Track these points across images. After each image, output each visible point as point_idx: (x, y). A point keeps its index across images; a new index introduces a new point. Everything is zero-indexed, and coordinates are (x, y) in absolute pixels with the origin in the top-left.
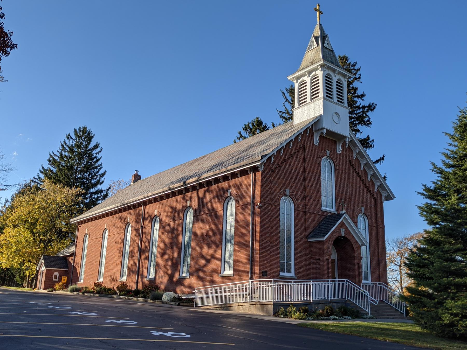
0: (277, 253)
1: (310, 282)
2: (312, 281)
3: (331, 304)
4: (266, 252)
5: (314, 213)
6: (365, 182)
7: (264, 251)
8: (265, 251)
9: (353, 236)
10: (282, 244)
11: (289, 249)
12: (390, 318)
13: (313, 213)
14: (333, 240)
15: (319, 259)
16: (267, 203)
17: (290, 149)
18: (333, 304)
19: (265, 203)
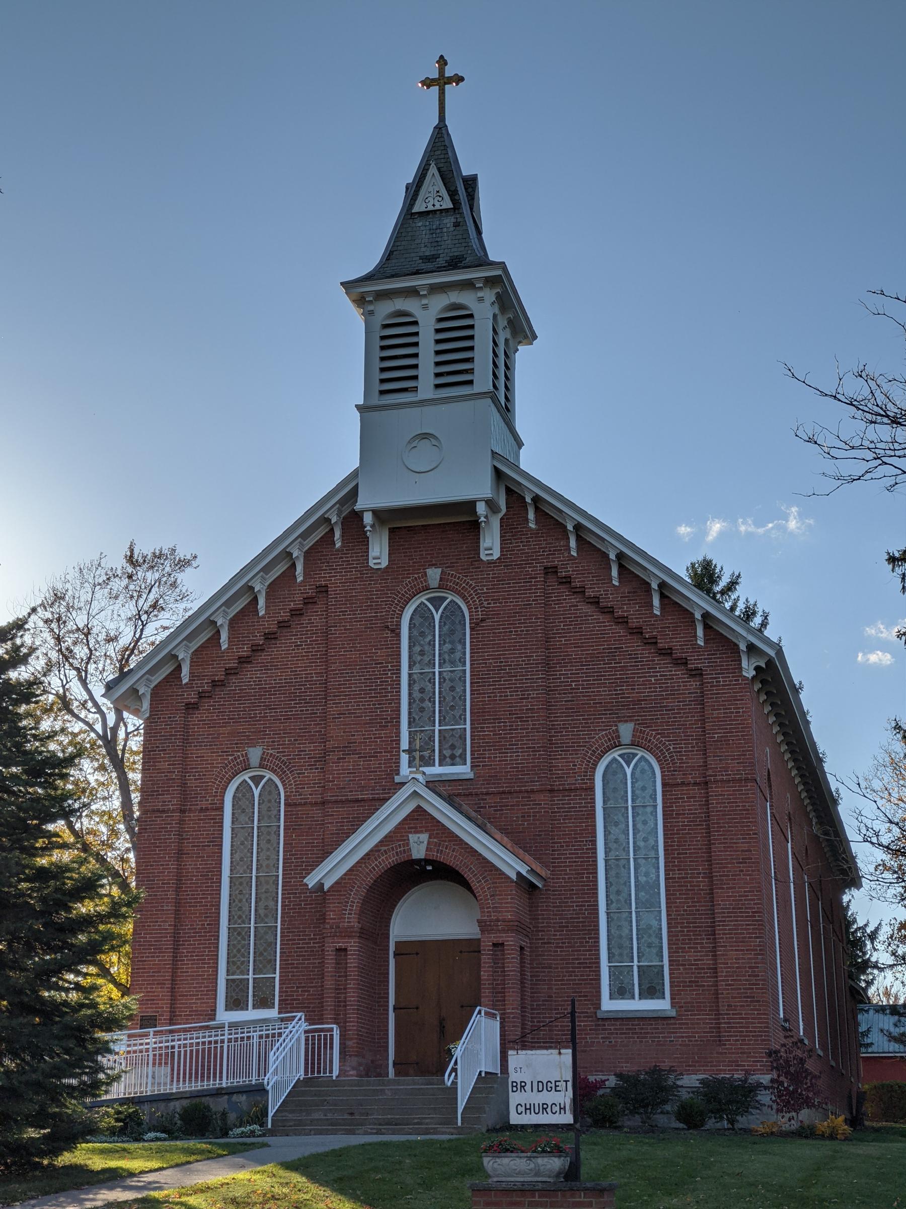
0: (207, 955)
1: (146, 1035)
2: (155, 1032)
3: (226, 1097)
4: (157, 957)
5: (363, 800)
6: (634, 625)
7: (146, 957)
8: (154, 957)
9: (367, 854)
10: (239, 921)
11: (266, 933)
12: (357, 1132)
13: (357, 801)
14: (370, 880)
15: (345, 950)
16: (163, 811)
17: (263, 617)
18: (235, 1098)
19: (158, 811)
